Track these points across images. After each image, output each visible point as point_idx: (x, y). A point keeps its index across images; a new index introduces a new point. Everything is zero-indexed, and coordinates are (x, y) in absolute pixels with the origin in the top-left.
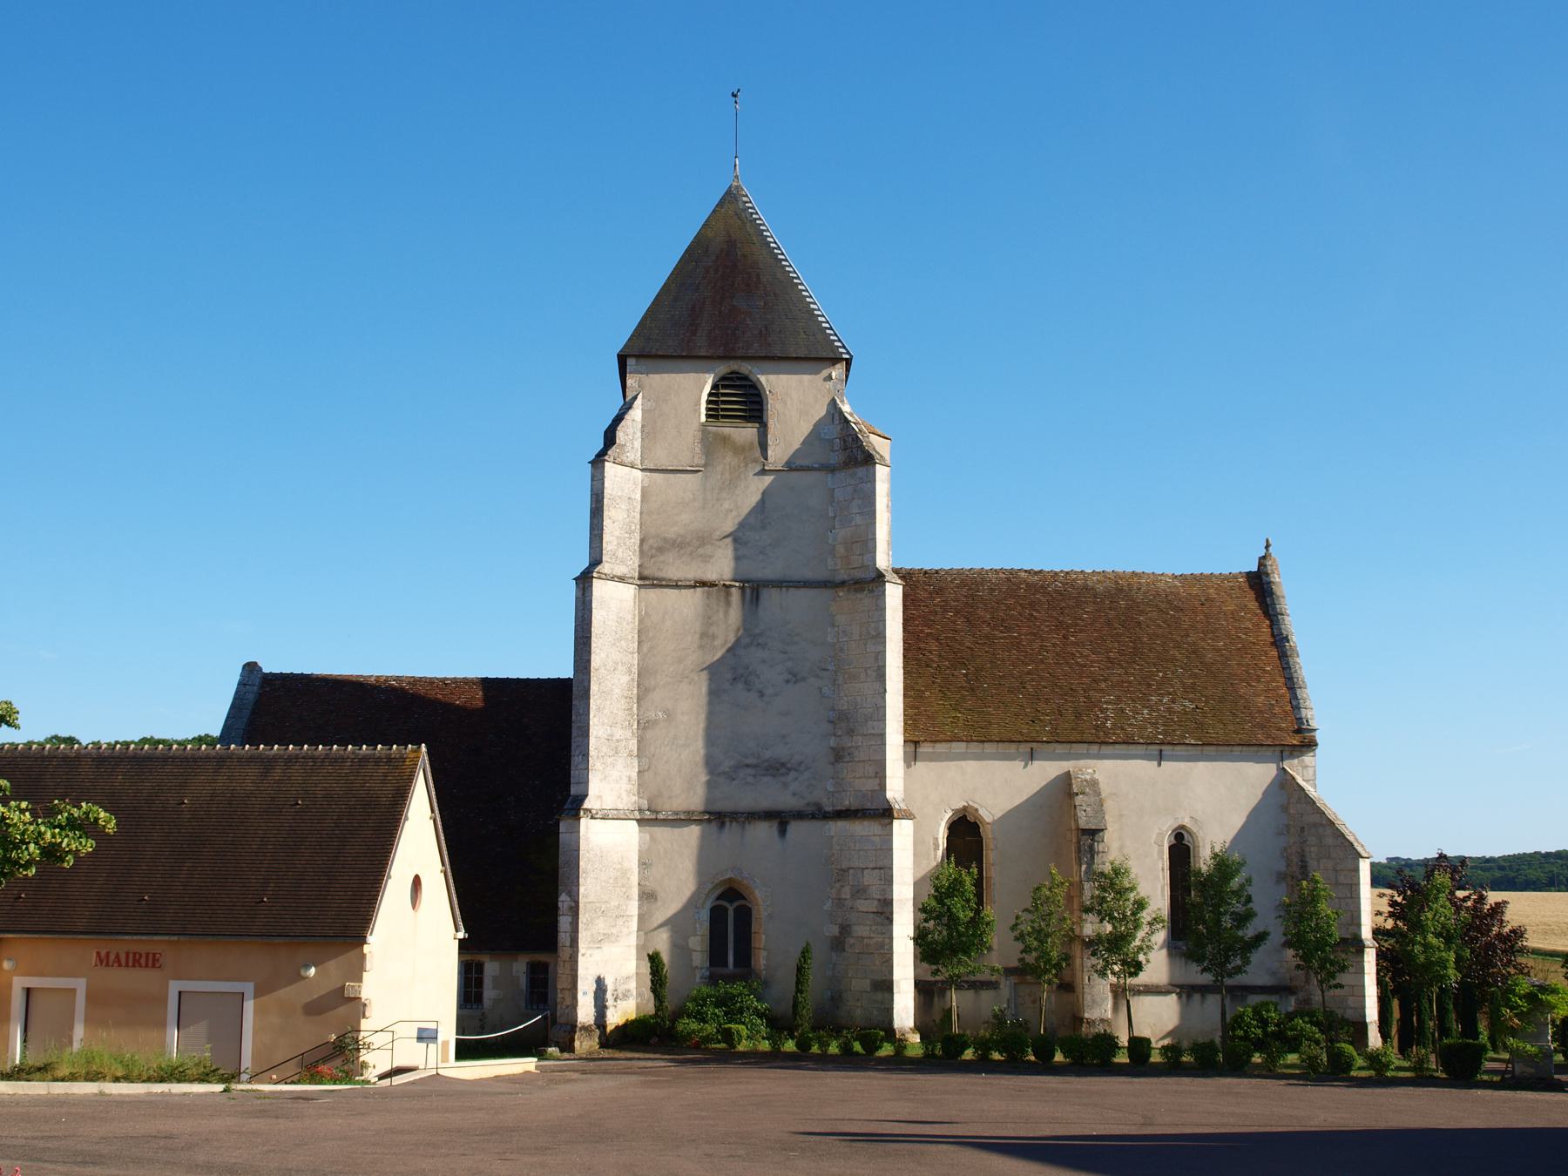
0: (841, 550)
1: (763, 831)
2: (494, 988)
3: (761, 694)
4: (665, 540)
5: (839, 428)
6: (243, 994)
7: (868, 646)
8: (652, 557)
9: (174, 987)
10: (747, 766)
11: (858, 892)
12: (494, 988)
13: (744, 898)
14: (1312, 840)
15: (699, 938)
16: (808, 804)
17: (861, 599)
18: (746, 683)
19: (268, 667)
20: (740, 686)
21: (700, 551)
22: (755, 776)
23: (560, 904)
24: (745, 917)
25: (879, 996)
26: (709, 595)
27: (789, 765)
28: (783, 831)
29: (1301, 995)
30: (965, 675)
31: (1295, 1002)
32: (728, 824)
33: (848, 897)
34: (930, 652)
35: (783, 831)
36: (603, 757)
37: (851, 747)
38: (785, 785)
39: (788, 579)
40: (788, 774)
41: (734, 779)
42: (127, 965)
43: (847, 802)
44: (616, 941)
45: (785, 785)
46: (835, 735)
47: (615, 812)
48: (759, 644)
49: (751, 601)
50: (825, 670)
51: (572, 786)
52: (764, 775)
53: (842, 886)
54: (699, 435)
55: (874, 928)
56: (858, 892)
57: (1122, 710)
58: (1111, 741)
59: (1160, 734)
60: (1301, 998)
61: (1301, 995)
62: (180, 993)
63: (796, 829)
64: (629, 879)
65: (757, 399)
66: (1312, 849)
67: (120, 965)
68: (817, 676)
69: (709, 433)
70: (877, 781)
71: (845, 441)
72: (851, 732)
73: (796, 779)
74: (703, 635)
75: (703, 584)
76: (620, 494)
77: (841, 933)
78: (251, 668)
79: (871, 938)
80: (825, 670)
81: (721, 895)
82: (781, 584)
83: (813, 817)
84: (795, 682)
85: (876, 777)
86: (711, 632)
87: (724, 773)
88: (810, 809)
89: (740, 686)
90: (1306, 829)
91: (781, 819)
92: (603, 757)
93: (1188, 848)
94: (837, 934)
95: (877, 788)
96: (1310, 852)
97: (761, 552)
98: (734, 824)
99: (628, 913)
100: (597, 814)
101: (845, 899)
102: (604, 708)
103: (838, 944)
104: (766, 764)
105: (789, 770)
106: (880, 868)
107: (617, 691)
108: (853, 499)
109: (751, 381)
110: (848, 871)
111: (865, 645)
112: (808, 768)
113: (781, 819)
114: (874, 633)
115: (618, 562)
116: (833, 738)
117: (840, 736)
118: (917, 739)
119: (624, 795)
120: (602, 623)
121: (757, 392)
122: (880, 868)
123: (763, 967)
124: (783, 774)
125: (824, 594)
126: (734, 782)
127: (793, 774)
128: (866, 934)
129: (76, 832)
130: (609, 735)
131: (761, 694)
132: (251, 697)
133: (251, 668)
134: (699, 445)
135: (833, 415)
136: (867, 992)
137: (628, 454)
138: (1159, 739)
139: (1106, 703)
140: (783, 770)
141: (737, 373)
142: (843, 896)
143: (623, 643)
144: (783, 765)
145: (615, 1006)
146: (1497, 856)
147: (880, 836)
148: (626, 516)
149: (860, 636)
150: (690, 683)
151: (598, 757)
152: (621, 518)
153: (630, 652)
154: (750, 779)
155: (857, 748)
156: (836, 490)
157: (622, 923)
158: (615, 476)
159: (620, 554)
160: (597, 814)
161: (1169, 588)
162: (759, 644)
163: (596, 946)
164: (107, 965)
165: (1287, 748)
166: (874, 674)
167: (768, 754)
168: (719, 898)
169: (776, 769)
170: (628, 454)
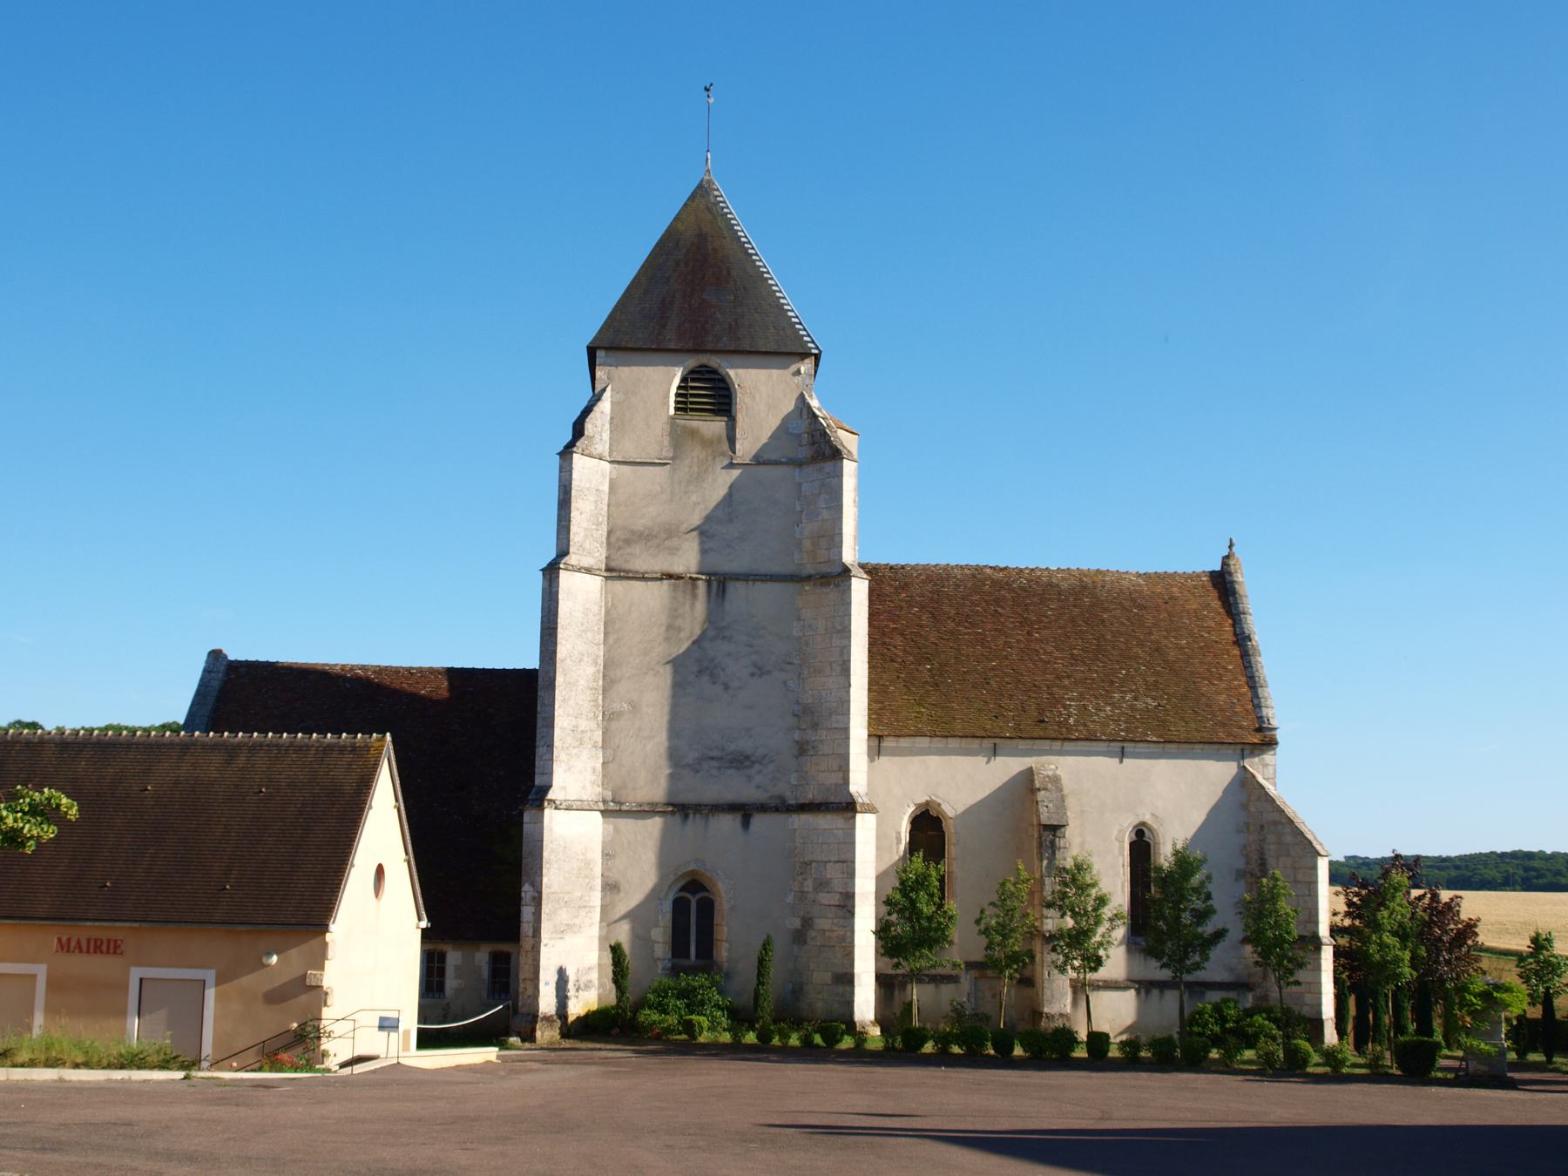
0: (807, 544)
1: (728, 824)
2: (456, 978)
3: (726, 687)
5: (807, 422)
7: (834, 640)
8: (620, 548)
9: (136, 973)
10: (712, 758)
11: (821, 885)
12: (456, 978)
13: (707, 891)
14: (1271, 838)
16: (772, 797)
17: (827, 594)
18: (711, 675)
20: (705, 678)
22: (719, 769)
23: (523, 895)
24: (707, 909)
25: (840, 989)
26: (675, 588)
27: (753, 758)
28: (746, 824)
29: (1258, 992)
30: (930, 670)
31: (1253, 999)
32: (691, 816)
33: (811, 889)
35: (746, 824)
36: (567, 748)
37: (815, 741)
38: (749, 778)
41: (698, 771)
43: (810, 795)
44: (579, 931)
45: (749, 778)
46: (799, 729)
47: (579, 803)
49: (717, 594)
50: (790, 663)
51: (536, 776)
54: (667, 428)
55: (835, 921)
56: (821, 885)
57: (1085, 707)
58: (1074, 737)
59: (1122, 730)
60: (1258, 995)
61: (1258, 992)
62: (141, 980)
63: (759, 821)
64: (592, 870)
65: (727, 393)
66: (1272, 847)
67: (81, 951)
69: (678, 426)
70: (841, 774)
71: (813, 436)
72: (815, 726)
73: (760, 772)
74: (669, 627)
75: (670, 576)
77: (802, 926)
78: (216, 656)
80: (790, 663)
83: (777, 809)
85: (839, 771)
87: (688, 765)
89: (705, 678)
90: (1266, 827)
91: (745, 811)
92: (567, 748)
93: (1148, 845)
96: (1269, 850)
97: (728, 546)
98: (698, 816)
99: (591, 904)
100: (561, 804)
101: (808, 892)
102: (569, 699)
103: (800, 937)
104: (731, 756)
106: (843, 862)
107: (582, 682)
108: (820, 493)
109: (719, 374)
110: (811, 864)
111: (831, 639)
113: (745, 811)
114: (839, 628)
117: (804, 730)
118: (880, 733)
119: (588, 785)
121: (725, 386)
122: (843, 862)
123: (724, 960)
124: (746, 767)
125: (791, 587)
127: (757, 767)
130: (574, 726)
131: (726, 687)
132: (216, 684)
133: (216, 656)
135: (802, 410)
136: (828, 985)
137: (597, 446)
138: (1121, 736)
139: (1069, 699)
140: (747, 763)
141: (706, 367)
142: (806, 889)
143: (589, 634)
144: (747, 758)
145: (577, 997)
148: (593, 508)
149: (826, 630)
151: (563, 748)
153: (596, 644)
154: (714, 772)
156: (804, 485)
157: (584, 914)
158: (583, 468)
159: (587, 545)
160: (561, 804)
161: (1133, 586)
163: (559, 936)
164: (68, 951)
166: (840, 668)
167: (732, 747)
168: (683, 889)
169: (740, 761)
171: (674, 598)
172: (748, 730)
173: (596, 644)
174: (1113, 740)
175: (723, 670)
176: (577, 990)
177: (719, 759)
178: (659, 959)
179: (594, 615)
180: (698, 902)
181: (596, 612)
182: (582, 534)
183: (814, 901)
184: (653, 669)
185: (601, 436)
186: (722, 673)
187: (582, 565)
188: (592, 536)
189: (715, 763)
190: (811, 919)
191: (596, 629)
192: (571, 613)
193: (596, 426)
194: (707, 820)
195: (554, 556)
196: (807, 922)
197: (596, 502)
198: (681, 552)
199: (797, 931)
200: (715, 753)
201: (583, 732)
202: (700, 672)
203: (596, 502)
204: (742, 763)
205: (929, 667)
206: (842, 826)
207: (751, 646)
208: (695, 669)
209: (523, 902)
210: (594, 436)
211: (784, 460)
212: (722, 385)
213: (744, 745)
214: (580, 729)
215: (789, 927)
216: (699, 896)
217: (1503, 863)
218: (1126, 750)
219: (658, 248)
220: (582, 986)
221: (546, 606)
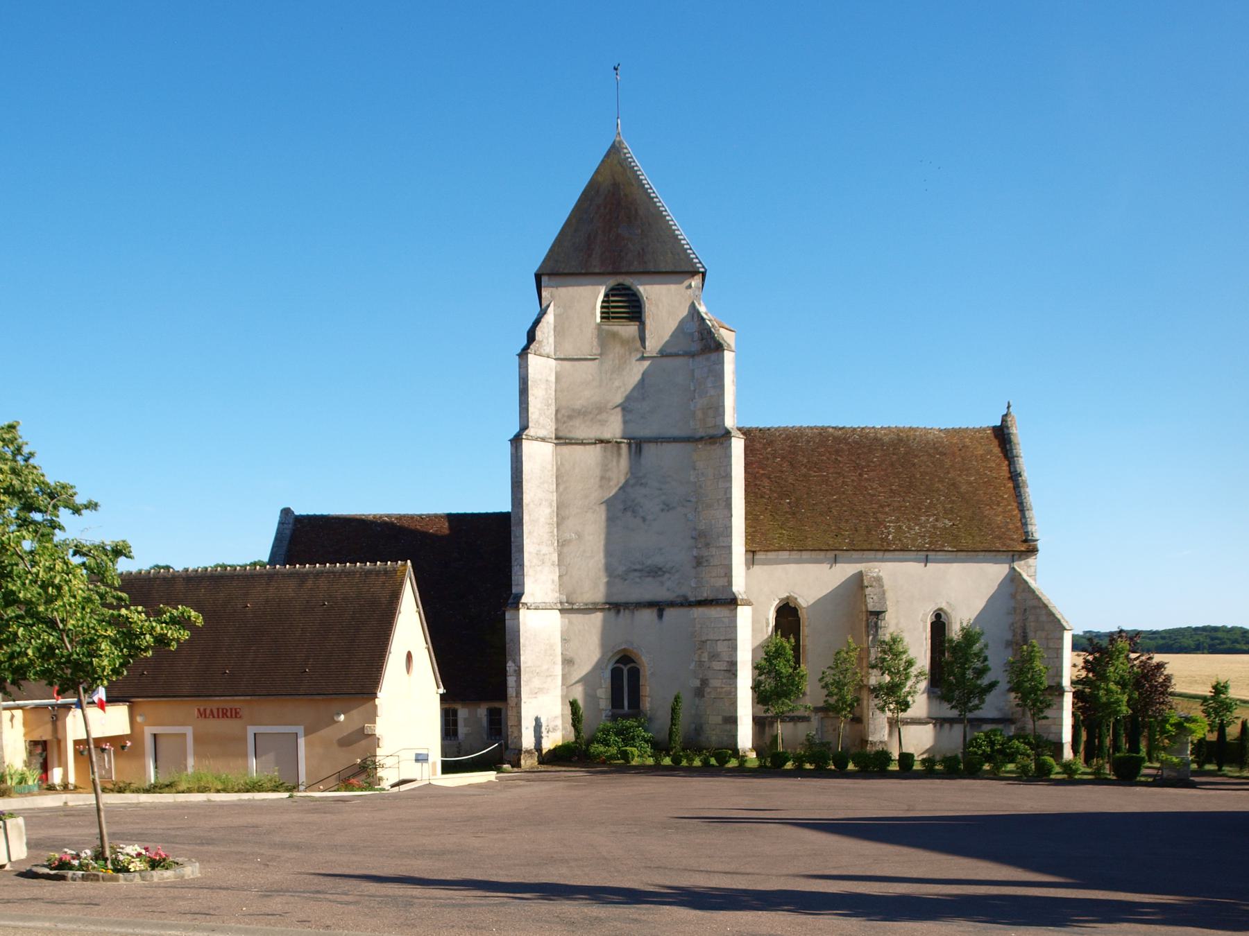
1: (648, 615)
3: (644, 519)
4: (573, 410)
6: (297, 734)
7: (720, 484)
8: (564, 423)
9: (251, 730)
10: (635, 570)
13: (635, 662)
15: (604, 690)
16: (678, 596)
18: (634, 511)
19: (299, 510)
21: (599, 417)
22: (640, 577)
24: (635, 674)
25: (728, 727)
26: (605, 448)
27: (664, 569)
28: (660, 616)
30: (789, 503)
33: (706, 660)
34: (764, 487)
35: (660, 616)
38: (662, 583)
40: (663, 575)
41: (626, 580)
42: (218, 717)
46: (696, 547)
48: (642, 484)
51: (513, 587)
52: (648, 576)
53: (702, 652)
54: (596, 332)
56: (713, 656)
57: (900, 527)
63: (670, 613)
67: (214, 717)
69: (603, 330)
72: (707, 545)
77: (701, 685)
79: (722, 688)
81: (618, 660)
83: (682, 605)
85: (725, 576)
94: (699, 685)
95: (726, 584)
101: (704, 662)
105: (664, 572)
109: (633, 290)
113: (659, 607)
114: (724, 474)
115: (540, 427)
116: (695, 549)
117: (700, 548)
122: (729, 640)
124: (660, 576)
125: (689, 447)
128: (719, 685)
131: (644, 519)
132: (288, 532)
134: (596, 340)
136: (720, 724)
138: (926, 547)
139: (889, 522)
141: (623, 285)
142: (703, 660)
144: (660, 569)
145: (548, 737)
147: (728, 617)
155: (712, 556)
164: (205, 717)
165: (1016, 553)
168: (617, 662)
169: (656, 572)
174: (920, 551)
176: (548, 732)
178: (603, 710)
180: (629, 670)
182: (537, 413)
183: (709, 667)
190: (707, 679)
196: (704, 682)
199: (698, 688)
201: (544, 555)
204: (656, 573)
205: (788, 501)
206: (728, 615)
209: (508, 674)
210: (542, 341)
212: (634, 298)
214: (542, 553)
215: (692, 686)
216: (629, 666)
220: (551, 729)
221: (514, 466)
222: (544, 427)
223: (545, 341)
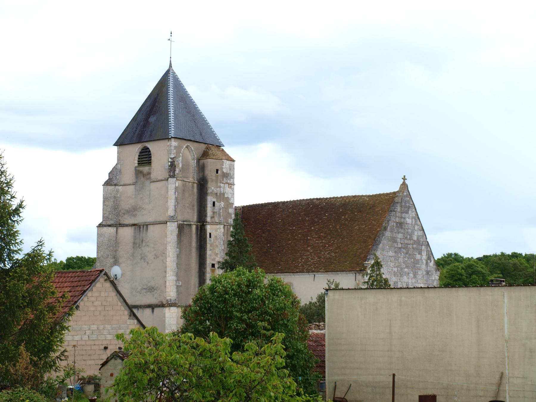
3: (148, 263)
4: (125, 210)
8: (122, 217)
10: (144, 289)
16: (159, 302)
18: (144, 259)
20: (143, 260)
22: (146, 292)
27: (154, 288)
32: (139, 309)
38: (153, 295)
39: (156, 221)
41: (141, 294)
45: (153, 295)
52: (148, 292)
54: (134, 171)
63: (156, 310)
68: (162, 256)
73: (156, 293)
74: (134, 243)
75: (134, 225)
76: (110, 196)
82: (154, 224)
84: (156, 258)
86: (403, 216)
87: (138, 292)
88: (160, 303)
89: (143, 260)
97: (149, 212)
98: (141, 309)
105: (155, 290)
112: (159, 289)
120: (101, 242)
124: (153, 291)
126: (141, 294)
127: (155, 291)
129: (180, 282)
131: (148, 263)
137: (114, 181)
143: (111, 248)
144: (153, 288)
146: (465, 257)
148: (113, 203)
150: (130, 260)
152: (110, 204)
153: (114, 251)
154: (145, 294)
158: (108, 190)
159: (110, 217)
162: (147, 245)
167: (149, 285)
170: (114, 181)
171: (135, 233)
172: (153, 278)
173: (114, 251)
175: (147, 257)
177: (146, 289)
179: (113, 241)
181: (114, 240)
182: (108, 213)
184: (130, 258)
185: (116, 177)
186: (147, 258)
187: (108, 224)
188: (112, 213)
189: (145, 291)
191: (114, 246)
192: (102, 242)
193: (114, 174)
194: (143, 310)
195: (102, 221)
197: (114, 201)
198: (137, 216)
200: (145, 287)
202: (141, 258)
203: (114, 201)
207: (154, 248)
208: (140, 257)
211: (163, 179)
213: (152, 284)
217: (109, 330)
218: (316, 276)
219: (335, 199)
222: (111, 220)
223: (114, 178)
